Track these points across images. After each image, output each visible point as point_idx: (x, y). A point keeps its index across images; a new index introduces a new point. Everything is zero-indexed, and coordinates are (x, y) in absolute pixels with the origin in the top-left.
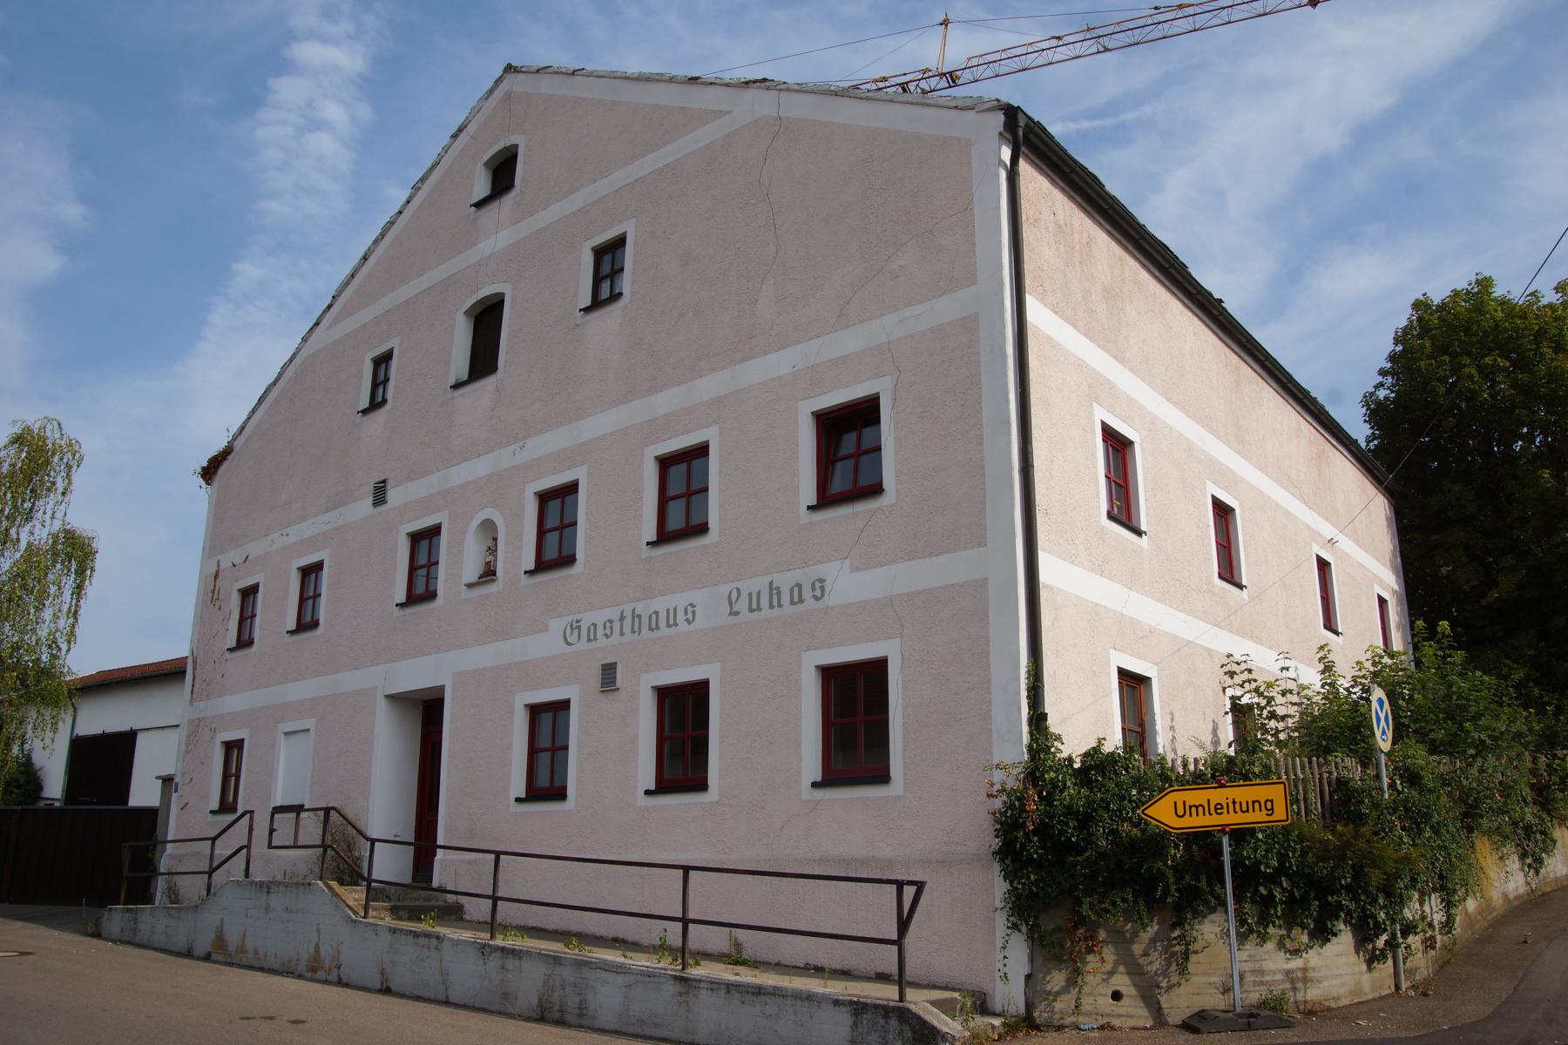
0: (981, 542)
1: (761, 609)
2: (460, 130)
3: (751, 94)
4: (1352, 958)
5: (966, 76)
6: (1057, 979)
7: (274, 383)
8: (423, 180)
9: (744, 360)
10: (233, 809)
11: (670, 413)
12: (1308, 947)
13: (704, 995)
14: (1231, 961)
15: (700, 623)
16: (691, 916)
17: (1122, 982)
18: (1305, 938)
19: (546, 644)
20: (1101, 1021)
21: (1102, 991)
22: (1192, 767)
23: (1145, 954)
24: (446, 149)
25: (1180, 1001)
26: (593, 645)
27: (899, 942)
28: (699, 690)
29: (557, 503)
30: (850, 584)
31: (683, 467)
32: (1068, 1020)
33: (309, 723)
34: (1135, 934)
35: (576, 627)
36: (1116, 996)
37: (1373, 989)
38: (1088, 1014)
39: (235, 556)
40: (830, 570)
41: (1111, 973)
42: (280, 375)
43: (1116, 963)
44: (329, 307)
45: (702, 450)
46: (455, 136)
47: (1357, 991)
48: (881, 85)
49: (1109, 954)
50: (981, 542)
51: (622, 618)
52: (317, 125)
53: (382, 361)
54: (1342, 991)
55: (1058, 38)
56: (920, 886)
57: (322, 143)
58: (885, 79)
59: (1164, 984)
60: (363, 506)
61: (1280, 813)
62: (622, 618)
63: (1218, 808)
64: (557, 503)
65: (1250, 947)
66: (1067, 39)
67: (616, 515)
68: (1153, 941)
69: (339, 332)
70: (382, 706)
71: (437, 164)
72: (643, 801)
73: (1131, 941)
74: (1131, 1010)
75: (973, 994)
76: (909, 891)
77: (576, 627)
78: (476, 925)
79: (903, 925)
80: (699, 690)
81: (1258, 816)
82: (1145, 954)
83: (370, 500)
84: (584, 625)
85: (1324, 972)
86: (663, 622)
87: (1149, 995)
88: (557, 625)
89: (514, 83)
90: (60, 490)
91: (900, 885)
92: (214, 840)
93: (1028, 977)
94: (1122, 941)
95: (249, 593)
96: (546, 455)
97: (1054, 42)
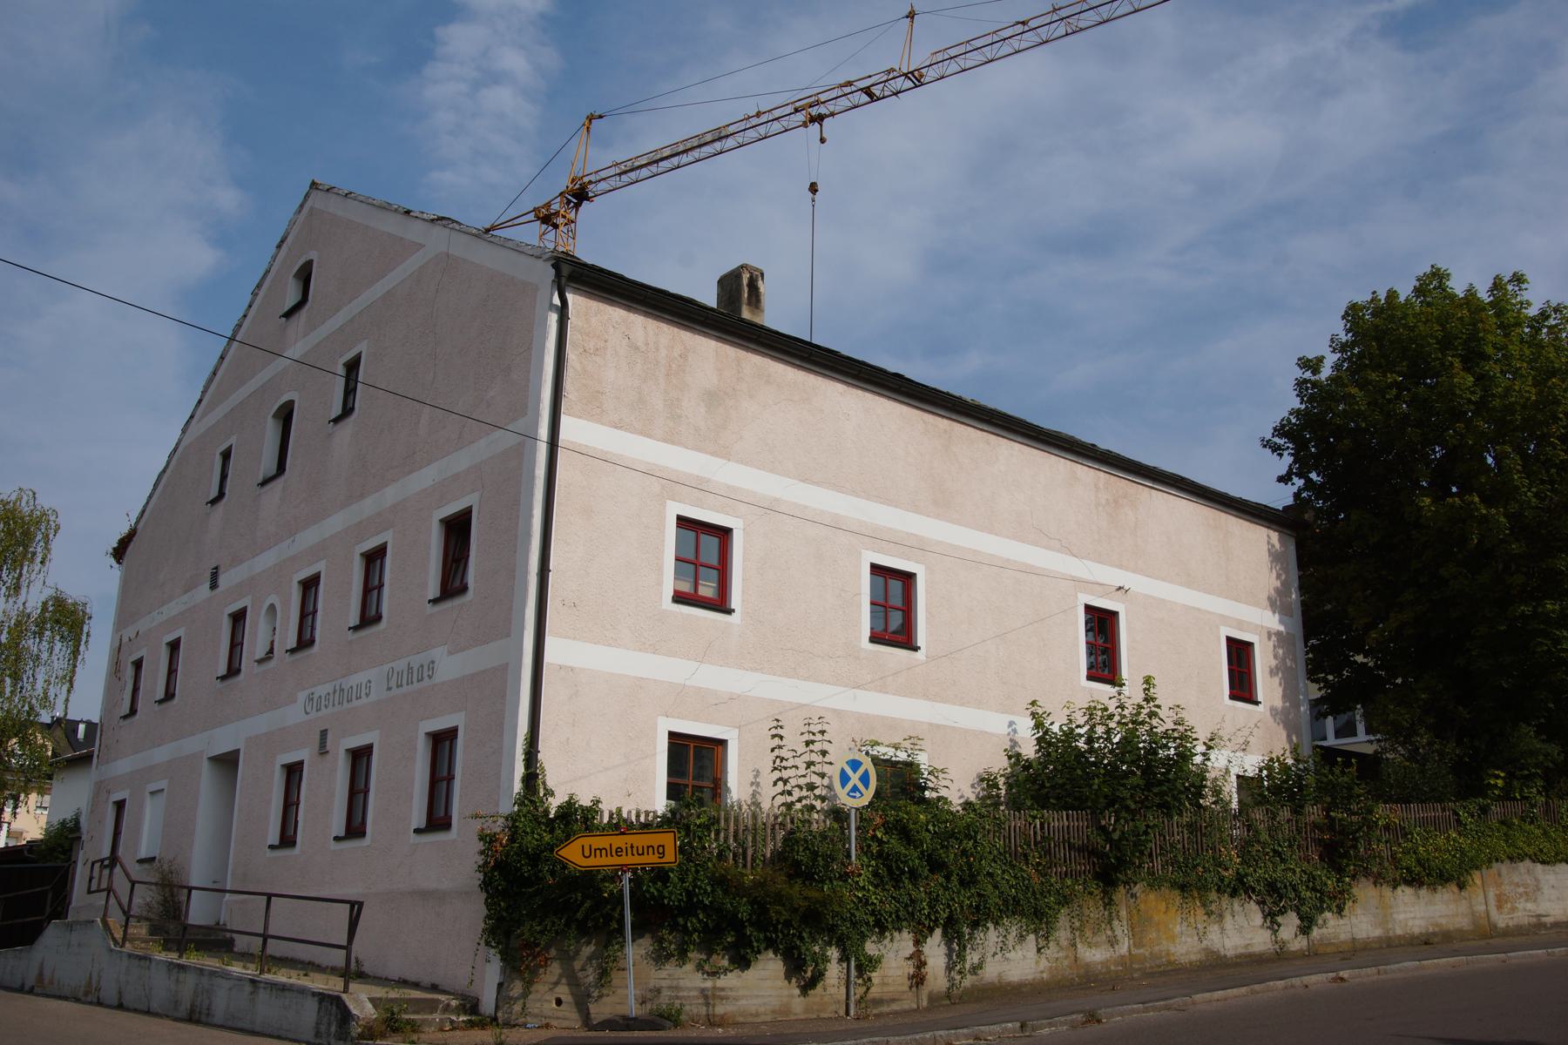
0: (508, 635)
1: (368, 692)
2: (282, 241)
3: (437, 230)
4: (782, 983)
5: (931, 74)
6: (517, 988)
7: (164, 471)
8: (259, 286)
9: (410, 472)
12: (726, 971)
13: (263, 995)
14: (641, 976)
15: (373, 697)
16: (271, 932)
17: (563, 991)
18: (725, 963)
19: (293, 714)
20: (544, 1021)
21: (548, 1001)
22: (642, 819)
23: (583, 969)
24: (274, 258)
25: (601, 1010)
27: (348, 948)
32: (521, 1020)
33: (163, 784)
34: (577, 953)
36: (559, 1002)
37: (807, 1011)
38: (536, 1016)
39: (129, 632)
40: (439, 653)
41: (556, 984)
42: (168, 463)
43: (561, 976)
44: (200, 401)
46: (279, 247)
47: (785, 1010)
48: (847, 90)
49: (555, 969)
50: (508, 635)
52: (492, 77)
54: (762, 1009)
55: (1023, 23)
56: (89, 892)
57: (502, 98)
58: (850, 84)
59: (595, 994)
60: (204, 590)
61: (670, 856)
63: (619, 851)
65: (670, 968)
66: (1033, 24)
68: (590, 959)
69: (211, 420)
70: (206, 767)
71: (268, 272)
73: (573, 959)
74: (567, 1014)
75: (463, 997)
78: (246, 957)
81: (653, 858)
82: (583, 969)
83: (208, 585)
84: (316, 696)
85: (741, 993)
87: (582, 1002)
89: (317, 200)
90: (39, 559)
93: (500, 985)
94: (567, 958)
95: (138, 665)
97: (1020, 28)
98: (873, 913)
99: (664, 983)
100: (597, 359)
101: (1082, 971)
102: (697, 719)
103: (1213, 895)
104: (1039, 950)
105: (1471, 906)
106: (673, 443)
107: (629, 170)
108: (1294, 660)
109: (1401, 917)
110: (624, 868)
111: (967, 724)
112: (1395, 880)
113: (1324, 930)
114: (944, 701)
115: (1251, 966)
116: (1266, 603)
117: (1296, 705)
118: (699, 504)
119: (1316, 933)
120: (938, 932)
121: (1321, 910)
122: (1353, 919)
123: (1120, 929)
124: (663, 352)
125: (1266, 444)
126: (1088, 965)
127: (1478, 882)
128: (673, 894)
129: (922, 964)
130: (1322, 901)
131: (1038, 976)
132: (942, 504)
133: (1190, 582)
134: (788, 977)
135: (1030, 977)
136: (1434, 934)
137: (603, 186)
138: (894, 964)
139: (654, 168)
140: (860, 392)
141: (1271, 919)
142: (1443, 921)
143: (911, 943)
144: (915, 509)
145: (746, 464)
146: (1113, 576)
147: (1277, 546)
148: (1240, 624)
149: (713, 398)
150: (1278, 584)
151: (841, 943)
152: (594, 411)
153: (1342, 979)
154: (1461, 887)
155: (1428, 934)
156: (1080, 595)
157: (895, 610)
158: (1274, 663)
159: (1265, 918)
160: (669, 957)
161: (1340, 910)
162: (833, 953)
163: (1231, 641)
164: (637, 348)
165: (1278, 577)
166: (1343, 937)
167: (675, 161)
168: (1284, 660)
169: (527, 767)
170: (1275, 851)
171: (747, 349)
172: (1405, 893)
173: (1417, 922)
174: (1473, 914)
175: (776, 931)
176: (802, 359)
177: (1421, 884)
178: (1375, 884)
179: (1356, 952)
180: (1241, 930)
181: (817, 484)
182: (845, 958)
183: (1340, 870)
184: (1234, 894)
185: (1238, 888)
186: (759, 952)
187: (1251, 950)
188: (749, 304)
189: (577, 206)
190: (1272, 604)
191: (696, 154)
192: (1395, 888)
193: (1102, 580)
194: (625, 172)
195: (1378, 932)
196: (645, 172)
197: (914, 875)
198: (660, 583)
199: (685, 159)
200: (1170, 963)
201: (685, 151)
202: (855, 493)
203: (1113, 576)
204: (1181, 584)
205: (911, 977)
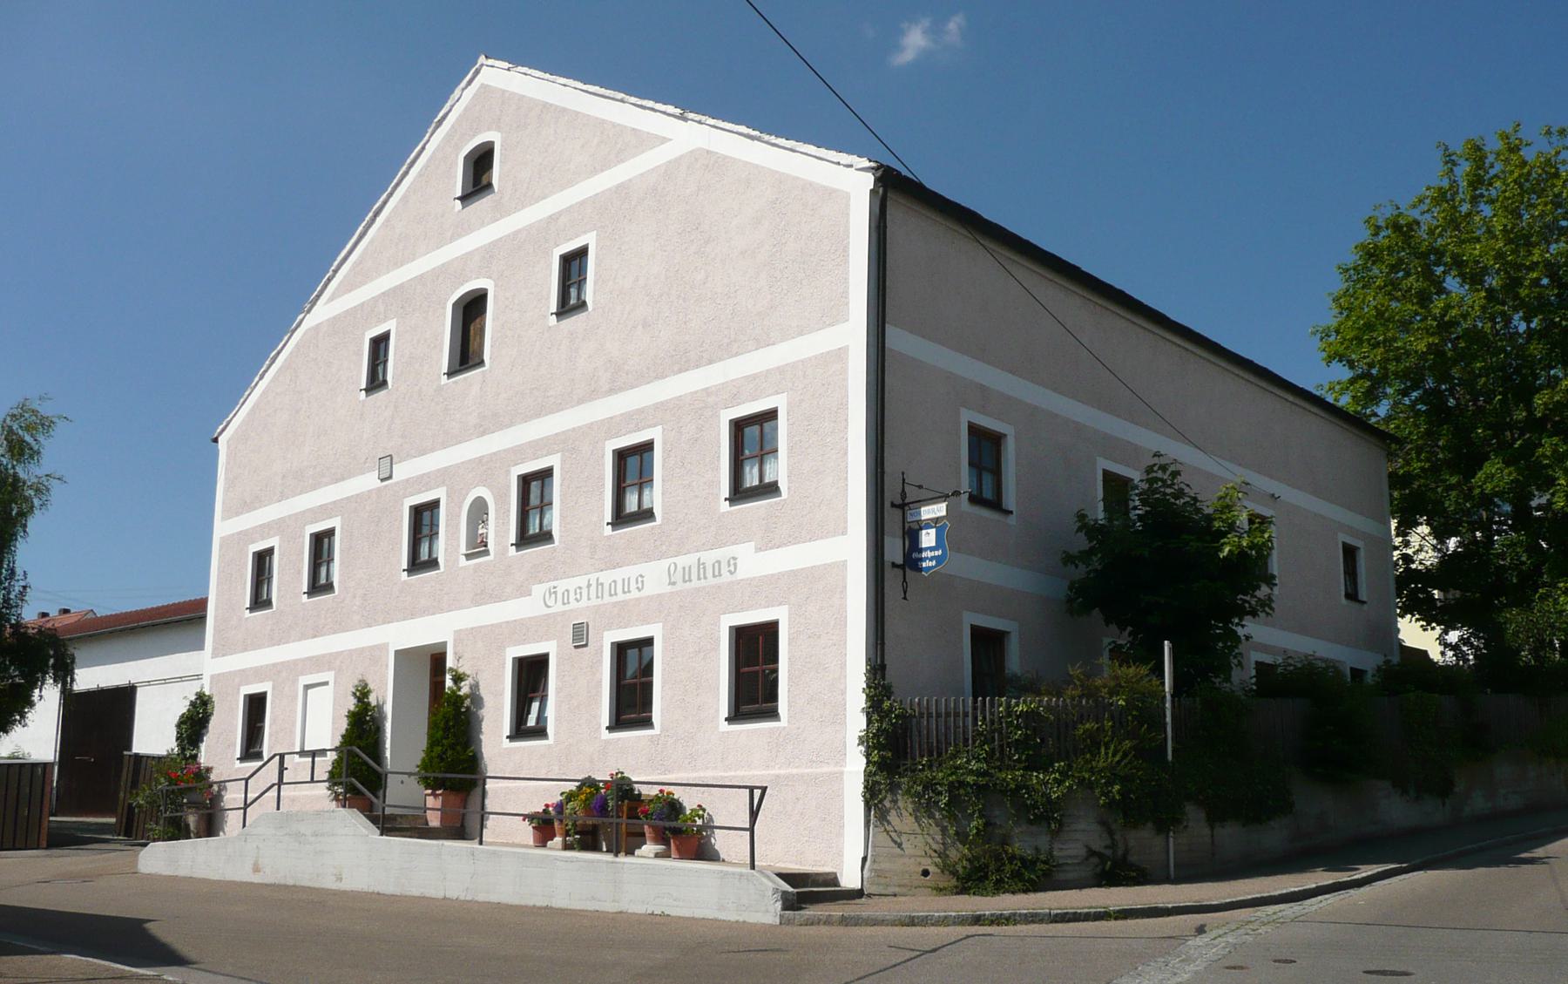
10: (259, 756)
11: (616, 415)
26: (567, 607)
27: (752, 830)
28: (769, 631)
29: (534, 487)
30: (753, 562)
31: (756, 428)
33: (328, 676)
35: (553, 592)
45: (771, 415)
51: (589, 586)
53: (379, 345)
62: (589, 586)
64: (534, 487)
67: (582, 502)
72: (606, 735)
76: (757, 793)
77: (553, 592)
79: (754, 815)
80: (769, 631)
86: (694, 576)
88: (539, 590)
91: (752, 789)
92: (247, 780)
96: (523, 441)
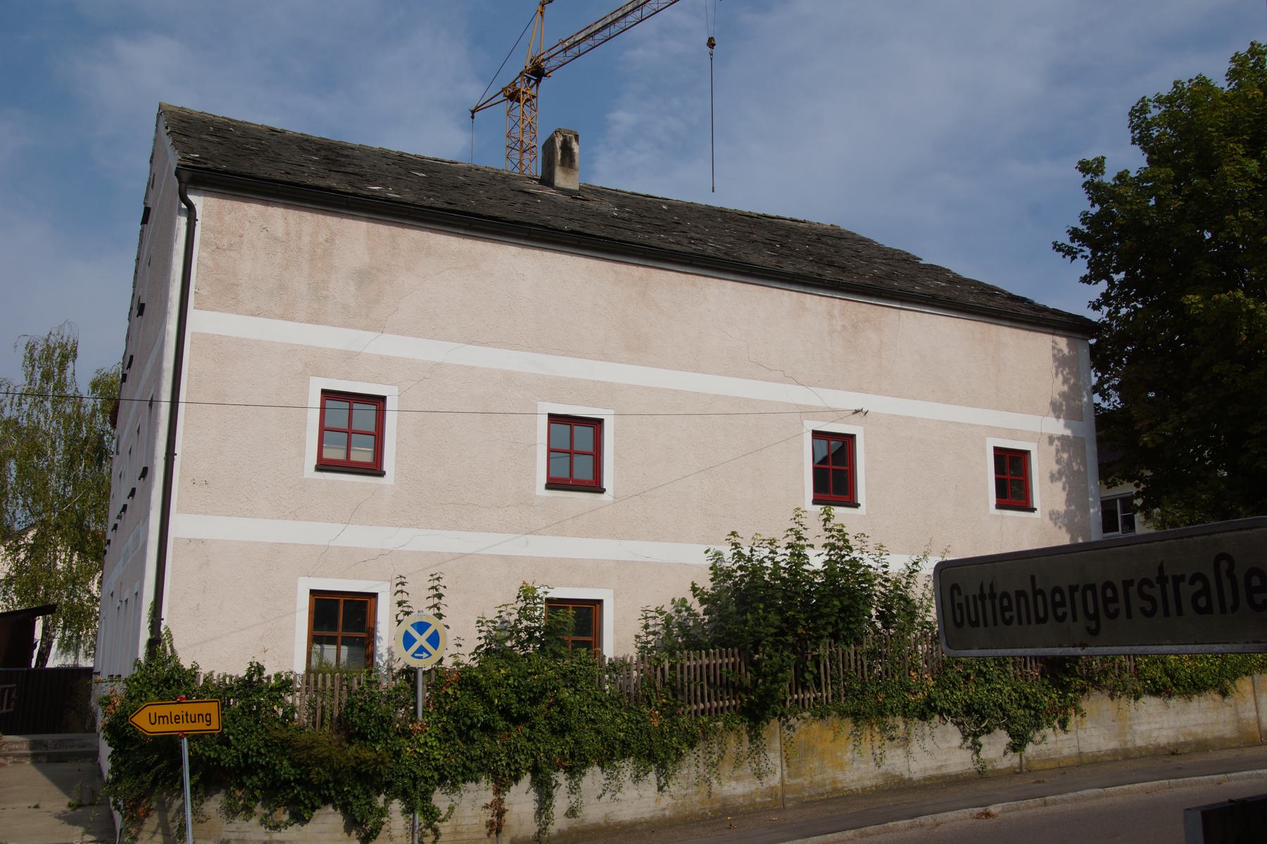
4: (341, 834)
12: (287, 825)
18: (286, 817)
41: (155, 833)
65: (238, 822)
98: (437, 769)
99: (233, 836)
100: (232, 254)
101: (717, 806)
102: (342, 576)
103: (899, 721)
104: (660, 789)
105: (1237, 713)
106: (317, 323)
107: (571, 48)
108: (1084, 463)
109: (1144, 728)
110: (184, 733)
111: (640, 567)
112: (1135, 691)
113: (1043, 746)
114: (633, 538)
115: (943, 788)
116: (1048, 408)
117: (1084, 508)
118: (347, 377)
119: (1030, 749)
120: (526, 779)
121: (1038, 727)
122: (1081, 733)
123: (774, 758)
124: (306, 239)
125: (1058, 247)
126: (725, 799)
127: (1249, 688)
128: (228, 758)
129: (501, 813)
130: (1036, 717)
131: (659, 814)
132: (637, 348)
133: (949, 397)
134: (348, 830)
135: (647, 816)
136: (1186, 744)
137: (553, 62)
138: (469, 813)
139: (590, 42)
140: (537, 252)
141: (973, 739)
142: (1199, 730)
143: (491, 793)
144: (605, 356)
145: (403, 334)
146: (849, 400)
147: (1066, 351)
148: (1012, 434)
149: (364, 277)
150: (1065, 388)
151: (404, 795)
152: (228, 298)
153: (988, 815)
154: (1224, 694)
155: (1177, 744)
156: (806, 422)
157: (576, 457)
158: (1055, 468)
159: (965, 738)
160: (235, 814)
161: (1063, 724)
162: (397, 806)
163: (1000, 453)
164: (276, 239)
165: (1065, 381)
166: (1066, 752)
167: (606, 33)
168: (1069, 464)
169: (152, 632)
170: (980, 671)
171: (403, 225)
172: (1150, 704)
173: (1165, 732)
174: (1239, 721)
175: (328, 789)
176: (465, 228)
177: (1170, 696)
178: (1112, 697)
179: (1087, 768)
180: (938, 750)
181: (483, 344)
182: (410, 810)
183: (1065, 688)
184: (923, 717)
185: (927, 711)
186: (314, 808)
187: (944, 771)
188: (563, 164)
189: (538, 82)
190: (1056, 409)
191: (622, 24)
192: (1136, 699)
193: (834, 407)
194: (568, 48)
195: (1113, 744)
196: (584, 46)
197: (487, 728)
198: (302, 454)
199: (614, 30)
200: (835, 790)
201: (613, 22)
202: (530, 349)
203: (849, 400)
204: (938, 401)
205: (490, 824)
